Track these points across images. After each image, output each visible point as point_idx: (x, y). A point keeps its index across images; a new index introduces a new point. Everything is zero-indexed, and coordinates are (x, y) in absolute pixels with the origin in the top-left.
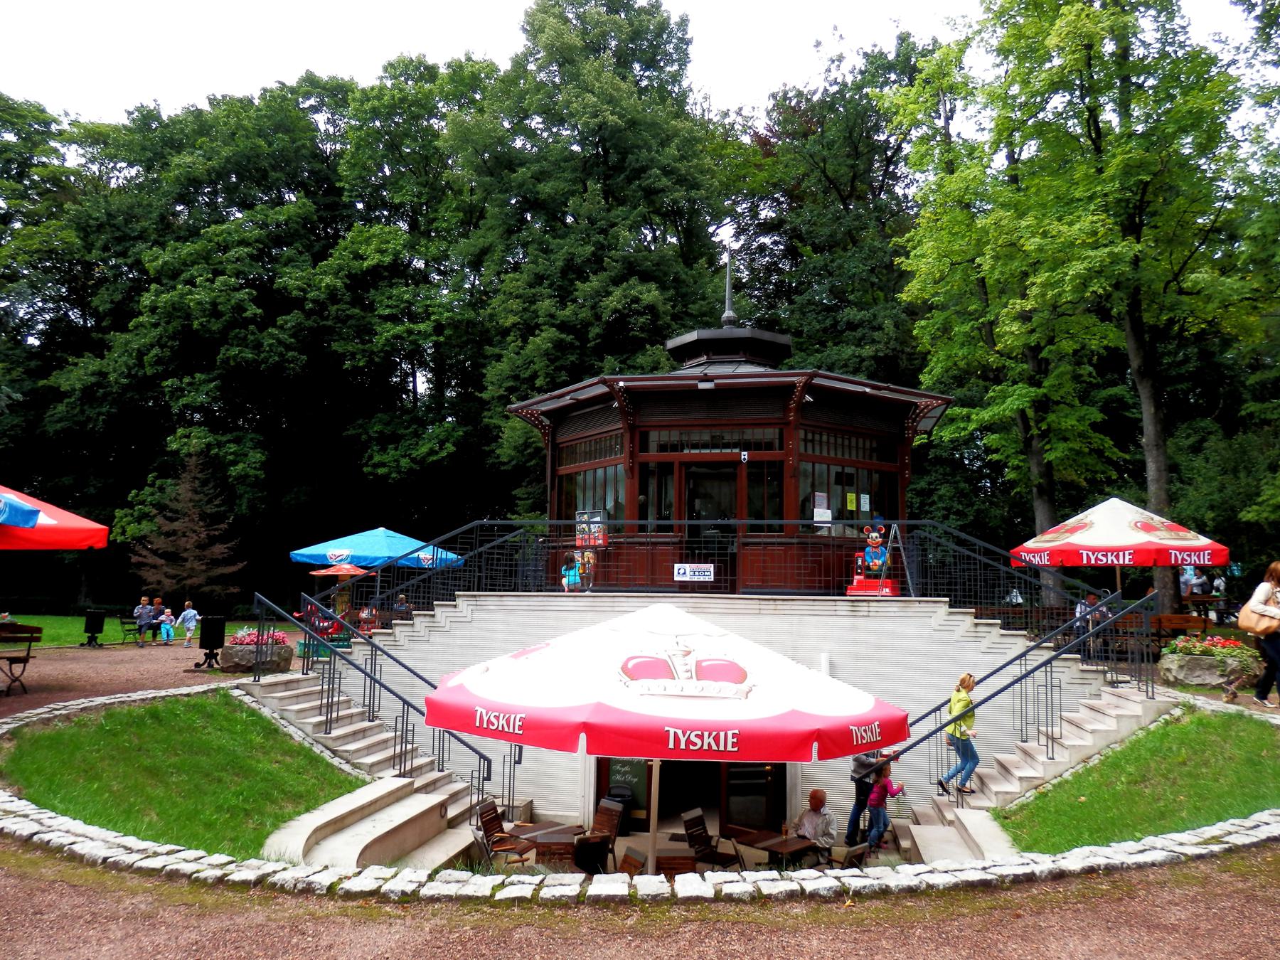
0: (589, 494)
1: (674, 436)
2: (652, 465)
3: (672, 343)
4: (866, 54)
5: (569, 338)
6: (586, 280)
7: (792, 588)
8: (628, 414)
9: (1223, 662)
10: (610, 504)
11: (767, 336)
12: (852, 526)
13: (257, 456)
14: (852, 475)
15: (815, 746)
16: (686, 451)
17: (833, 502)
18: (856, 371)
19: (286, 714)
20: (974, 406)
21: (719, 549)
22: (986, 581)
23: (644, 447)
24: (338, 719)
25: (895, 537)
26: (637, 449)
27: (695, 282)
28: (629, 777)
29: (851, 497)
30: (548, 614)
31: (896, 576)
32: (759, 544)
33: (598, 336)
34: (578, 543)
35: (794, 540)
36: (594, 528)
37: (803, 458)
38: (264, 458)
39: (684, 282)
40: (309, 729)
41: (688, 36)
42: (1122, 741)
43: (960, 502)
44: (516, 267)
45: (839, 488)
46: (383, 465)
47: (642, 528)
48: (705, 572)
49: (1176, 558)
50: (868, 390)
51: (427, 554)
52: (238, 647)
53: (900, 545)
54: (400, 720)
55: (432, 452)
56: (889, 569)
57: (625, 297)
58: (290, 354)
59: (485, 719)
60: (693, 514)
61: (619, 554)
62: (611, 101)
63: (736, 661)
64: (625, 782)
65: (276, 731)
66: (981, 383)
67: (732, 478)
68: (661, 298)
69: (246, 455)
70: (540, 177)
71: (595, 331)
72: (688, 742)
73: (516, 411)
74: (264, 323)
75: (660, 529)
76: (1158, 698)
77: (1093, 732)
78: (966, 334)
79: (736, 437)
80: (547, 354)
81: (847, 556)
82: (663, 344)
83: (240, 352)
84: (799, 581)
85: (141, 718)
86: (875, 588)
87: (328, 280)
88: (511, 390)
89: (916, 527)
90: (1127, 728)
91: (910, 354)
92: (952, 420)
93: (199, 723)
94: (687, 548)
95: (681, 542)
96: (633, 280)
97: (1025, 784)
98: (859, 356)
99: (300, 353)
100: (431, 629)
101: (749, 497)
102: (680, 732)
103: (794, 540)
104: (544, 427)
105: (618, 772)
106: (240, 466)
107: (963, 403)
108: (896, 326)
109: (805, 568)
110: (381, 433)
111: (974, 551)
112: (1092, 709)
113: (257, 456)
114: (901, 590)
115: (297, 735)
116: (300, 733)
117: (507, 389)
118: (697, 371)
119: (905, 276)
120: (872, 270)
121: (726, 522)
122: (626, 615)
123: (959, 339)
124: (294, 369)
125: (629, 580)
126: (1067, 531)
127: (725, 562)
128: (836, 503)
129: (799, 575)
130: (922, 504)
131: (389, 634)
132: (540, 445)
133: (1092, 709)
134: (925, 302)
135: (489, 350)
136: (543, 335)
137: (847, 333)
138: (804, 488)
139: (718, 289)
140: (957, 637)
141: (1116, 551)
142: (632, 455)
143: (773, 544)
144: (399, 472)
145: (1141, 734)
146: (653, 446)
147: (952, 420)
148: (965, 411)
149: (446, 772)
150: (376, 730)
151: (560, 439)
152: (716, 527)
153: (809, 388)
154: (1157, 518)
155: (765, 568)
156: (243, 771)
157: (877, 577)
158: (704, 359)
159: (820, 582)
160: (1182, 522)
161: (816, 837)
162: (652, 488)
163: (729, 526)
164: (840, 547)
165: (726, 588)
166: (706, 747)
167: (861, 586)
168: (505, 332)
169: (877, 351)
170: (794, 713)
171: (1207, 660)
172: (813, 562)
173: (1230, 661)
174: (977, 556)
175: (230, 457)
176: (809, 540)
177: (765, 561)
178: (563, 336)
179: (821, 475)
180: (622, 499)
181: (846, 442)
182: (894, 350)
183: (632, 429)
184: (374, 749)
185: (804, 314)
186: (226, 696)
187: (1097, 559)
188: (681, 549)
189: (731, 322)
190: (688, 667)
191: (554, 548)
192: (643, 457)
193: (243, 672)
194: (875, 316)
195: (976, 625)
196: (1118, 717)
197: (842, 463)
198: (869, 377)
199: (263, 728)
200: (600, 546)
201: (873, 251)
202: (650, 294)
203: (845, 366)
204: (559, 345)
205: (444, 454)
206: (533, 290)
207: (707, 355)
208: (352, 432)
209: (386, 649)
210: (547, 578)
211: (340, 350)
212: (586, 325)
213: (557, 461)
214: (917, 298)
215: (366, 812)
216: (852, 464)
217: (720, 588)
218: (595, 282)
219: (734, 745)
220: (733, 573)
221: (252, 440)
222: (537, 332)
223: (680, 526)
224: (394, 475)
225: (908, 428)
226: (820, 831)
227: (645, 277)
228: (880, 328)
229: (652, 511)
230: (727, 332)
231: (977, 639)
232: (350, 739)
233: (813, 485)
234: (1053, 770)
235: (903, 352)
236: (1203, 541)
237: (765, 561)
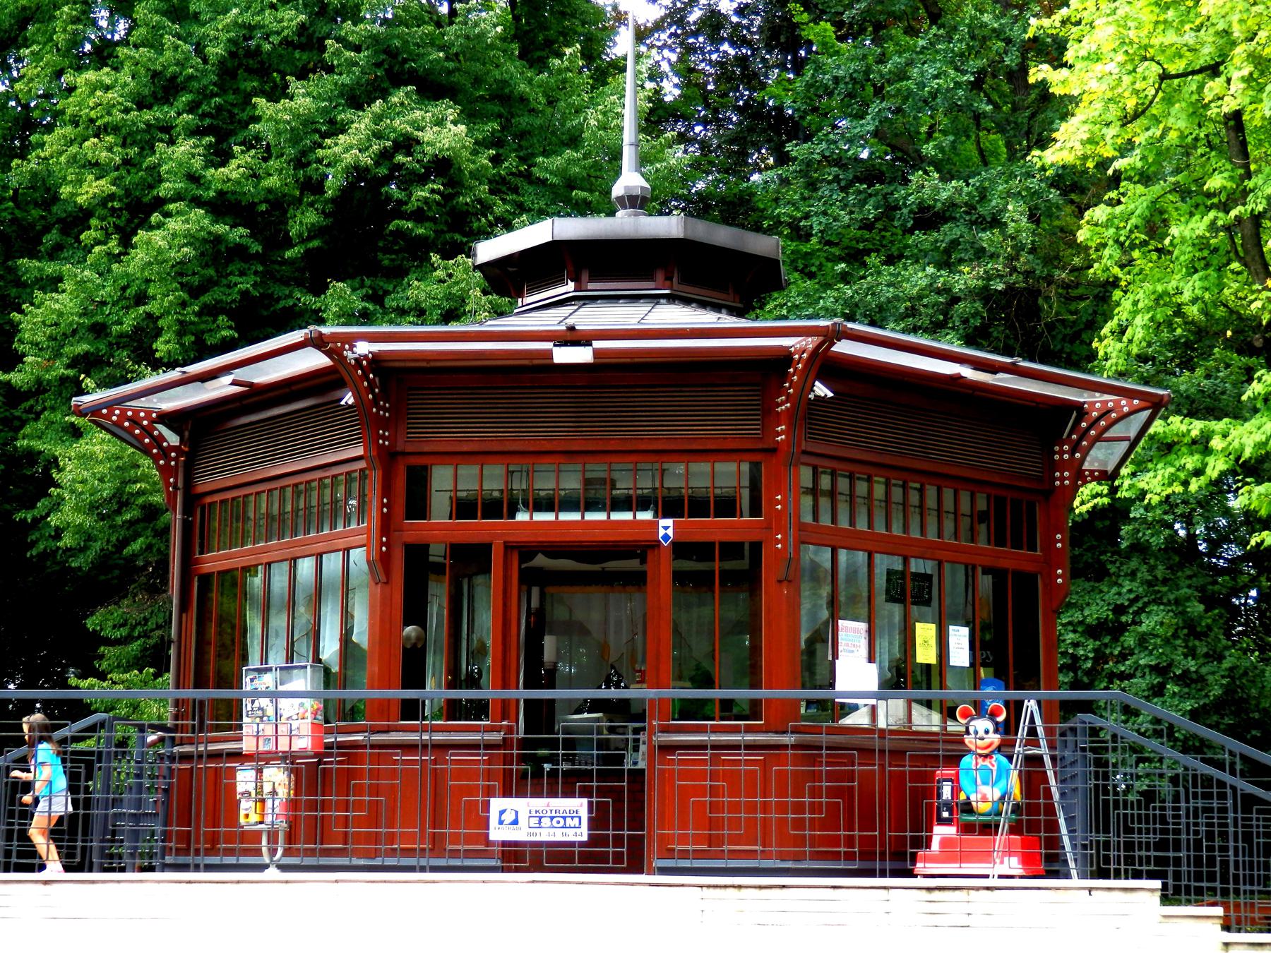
0: (279, 622)
1: (493, 480)
2: (437, 552)
3: (489, 250)
5: (238, 234)
6: (277, 93)
8: (384, 423)
10: (330, 648)
11: (722, 235)
12: (928, 704)
14: (927, 578)
16: (522, 517)
17: (882, 644)
18: (935, 328)
20: (1214, 412)
21: (603, 760)
22: (1248, 837)
23: (418, 506)
27: (551, 102)
29: (925, 633)
31: (1033, 827)
32: (701, 747)
33: (315, 232)
34: (247, 746)
35: (789, 739)
36: (288, 707)
37: (808, 535)
39: (523, 99)
43: (1192, 653)
44: (104, 54)
45: (897, 609)
47: (411, 710)
53: (1044, 750)
56: (1016, 809)
57: (378, 135)
60: (539, 675)
61: (351, 774)
66: (1238, 360)
68: (469, 142)
71: (305, 219)
73: (95, 411)
75: (454, 710)
78: (1201, 244)
79: (646, 483)
80: (180, 269)
81: (916, 777)
82: (470, 253)
84: (800, 841)
86: (986, 856)
88: (86, 363)
89: (1087, 706)
91: (1066, 286)
92: (1167, 448)
94: (522, 759)
95: (506, 744)
98: (946, 290)
101: (676, 631)
103: (789, 739)
104: (165, 453)
107: (1196, 407)
108: (1033, 217)
109: (814, 808)
111: (1220, 765)
117: (75, 362)
118: (552, 320)
119: (1063, 107)
120: (977, 85)
121: (613, 693)
123: (1184, 254)
125: (376, 838)
127: (617, 794)
128: (889, 647)
129: (799, 824)
130: (1100, 657)
132: (158, 499)
134: (1103, 164)
135: (28, 266)
136: (174, 224)
138: (812, 606)
139: (609, 124)
142: (386, 525)
143: (735, 747)
146: (440, 504)
147: (1167, 448)
148: (1197, 427)
151: (205, 483)
152: (595, 705)
155: (714, 807)
157: (988, 828)
159: (850, 841)
162: (437, 609)
163: (625, 703)
164: (898, 754)
165: (618, 858)
167: (951, 852)
168: (81, 218)
169: (988, 277)
172: (832, 792)
174: (1226, 777)
176: (824, 738)
177: (714, 791)
178: (221, 228)
179: (852, 575)
180: (361, 634)
181: (914, 498)
182: (1028, 274)
183: (387, 459)
185: (812, 186)
188: (507, 760)
189: (636, 202)
191: (186, 758)
192: (414, 530)
194: (983, 195)
198: (969, 341)
200: (302, 754)
201: (980, 38)
203: (912, 312)
206: (148, 115)
207: (576, 279)
210: (167, 836)
212: (279, 205)
213: (195, 539)
214: (1085, 158)
216: (925, 550)
217: (603, 858)
220: (637, 823)
222: (155, 218)
223: (505, 703)
225: (1062, 466)
228: (995, 222)
229: (435, 665)
230: (625, 224)
233: (833, 602)
235: (1049, 280)
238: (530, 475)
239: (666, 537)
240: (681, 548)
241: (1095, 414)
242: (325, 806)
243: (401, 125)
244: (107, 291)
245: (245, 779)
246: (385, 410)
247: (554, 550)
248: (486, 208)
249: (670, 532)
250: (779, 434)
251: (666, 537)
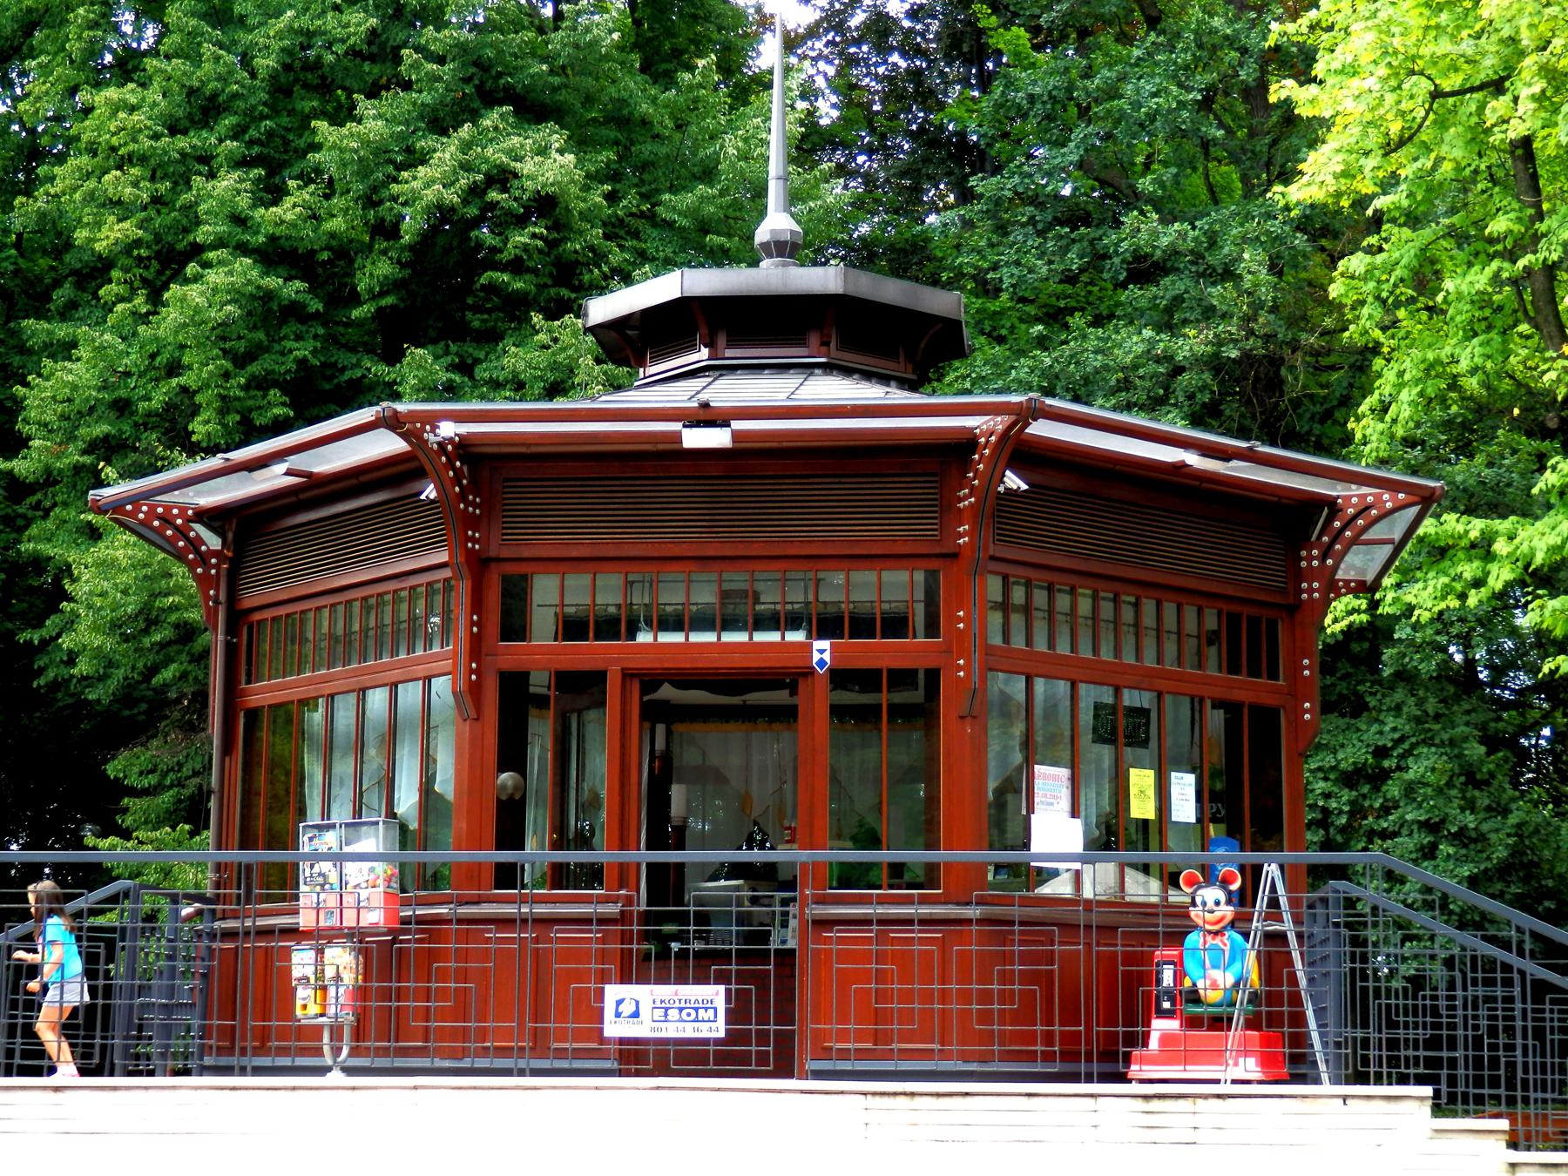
8: (471, 522)
33: (388, 287)
47: (507, 876)
57: (466, 167)
142: (476, 648)
146: (542, 622)
151: (250, 599)
183: (478, 566)
225: (1311, 574)
230: (771, 277)
239: (822, 662)
240: (840, 677)
241: (1351, 511)
243: (495, 154)
244: (133, 359)
245: (302, 961)
246: (475, 506)
248: (599, 256)
249: (827, 657)
250: (961, 536)
251: (822, 662)
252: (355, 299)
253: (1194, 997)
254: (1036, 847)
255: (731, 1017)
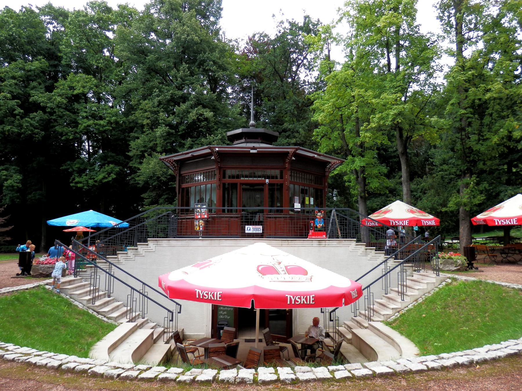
4: (289, 22)
7: (287, 235)
8: (219, 162)
9: (456, 261)
13: (18, 177)
15: (343, 300)
19: (73, 296)
24: (98, 296)
25: (334, 215)
26: (222, 177)
28: (226, 317)
30: (191, 248)
33: (183, 130)
38: (21, 178)
40: (85, 303)
41: (221, 7)
42: (429, 293)
46: (80, 183)
47: (224, 211)
48: (259, 229)
49: (498, 222)
50: (316, 156)
51: (111, 222)
52: (42, 266)
54: (129, 296)
55: (104, 178)
57: (197, 114)
58: (36, 130)
59: (201, 295)
62: (195, 30)
63: (300, 266)
64: (224, 318)
65: (71, 304)
67: (262, 190)
69: (12, 176)
70: (158, 59)
71: (182, 128)
72: (295, 301)
74: (25, 115)
76: (441, 276)
77: (418, 289)
83: (11, 128)
85: (12, 301)
87: (59, 99)
90: (431, 287)
93: (38, 302)
96: (200, 107)
97: (394, 311)
99: (41, 130)
100: (136, 255)
102: (292, 297)
105: (222, 314)
106: (9, 182)
110: (79, 168)
112: (412, 280)
113: (18, 177)
114: (333, 236)
115: (80, 306)
116: (81, 304)
122: (244, 248)
124: (38, 138)
126: (383, 213)
131: (116, 258)
133: (412, 280)
137: (283, 133)
140: (359, 254)
141: (509, 219)
142: (220, 180)
144: (88, 186)
145: (437, 289)
146: (227, 176)
149: (146, 319)
150: (112, 301)
151: (182, 173)
153: (295, 154)
154: (414, 208)
156: (66, 325)
158: (243, 140)
160: (423, 209)
161: (317, 336)
166: (302, 303)
170: (332, 287)
171: (451, 261)
173: (458, 261)
175: (4, 177)
177: (284, 225)
183: (220, 168)
184: (114, 310)
186: (44, 289)
187: (502, 222)
189: (253, 126)
190: (282, 269)
191: (181, 219)
193: (44, 277)
194: (295, 127)
195: (366, 249)
196: (427, 283)
197: (304, 185)
199: (66, 303)
200: (205, 218)
202: (208, 114)
204: (169, 134)
205: (110, 179)
208: (64, 167)
209: (115, 264)
211: (60, 130)
215: (123, 339)
218: (183, 106)
219: (313, 301)
221: (14, 169)
223: (237, 210)
224: (85, 187)
225: (327, 172)
226: (318, 335)
227: (204, 107)
230: (251, 130)
231: (366, 255)
232: (103, 306)
234: (405, 305)
236: (431, 217)
237: (284, 225)
238: (242, 172)
240: (270, 184)
242: (214, 227)
243: (200, 112)
244: (147, 139)
245: (196, 223)
247: (247, 184)
248: (213, 127)
252: (179, 132)
253: (317, 227)
254: (295, 207)
255: (263, 230)
